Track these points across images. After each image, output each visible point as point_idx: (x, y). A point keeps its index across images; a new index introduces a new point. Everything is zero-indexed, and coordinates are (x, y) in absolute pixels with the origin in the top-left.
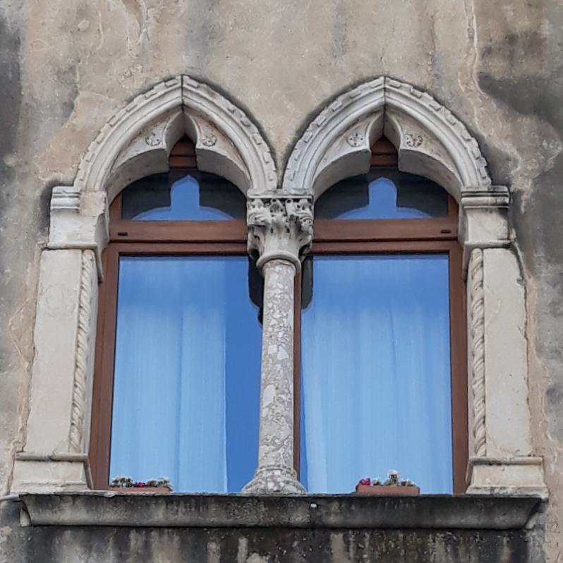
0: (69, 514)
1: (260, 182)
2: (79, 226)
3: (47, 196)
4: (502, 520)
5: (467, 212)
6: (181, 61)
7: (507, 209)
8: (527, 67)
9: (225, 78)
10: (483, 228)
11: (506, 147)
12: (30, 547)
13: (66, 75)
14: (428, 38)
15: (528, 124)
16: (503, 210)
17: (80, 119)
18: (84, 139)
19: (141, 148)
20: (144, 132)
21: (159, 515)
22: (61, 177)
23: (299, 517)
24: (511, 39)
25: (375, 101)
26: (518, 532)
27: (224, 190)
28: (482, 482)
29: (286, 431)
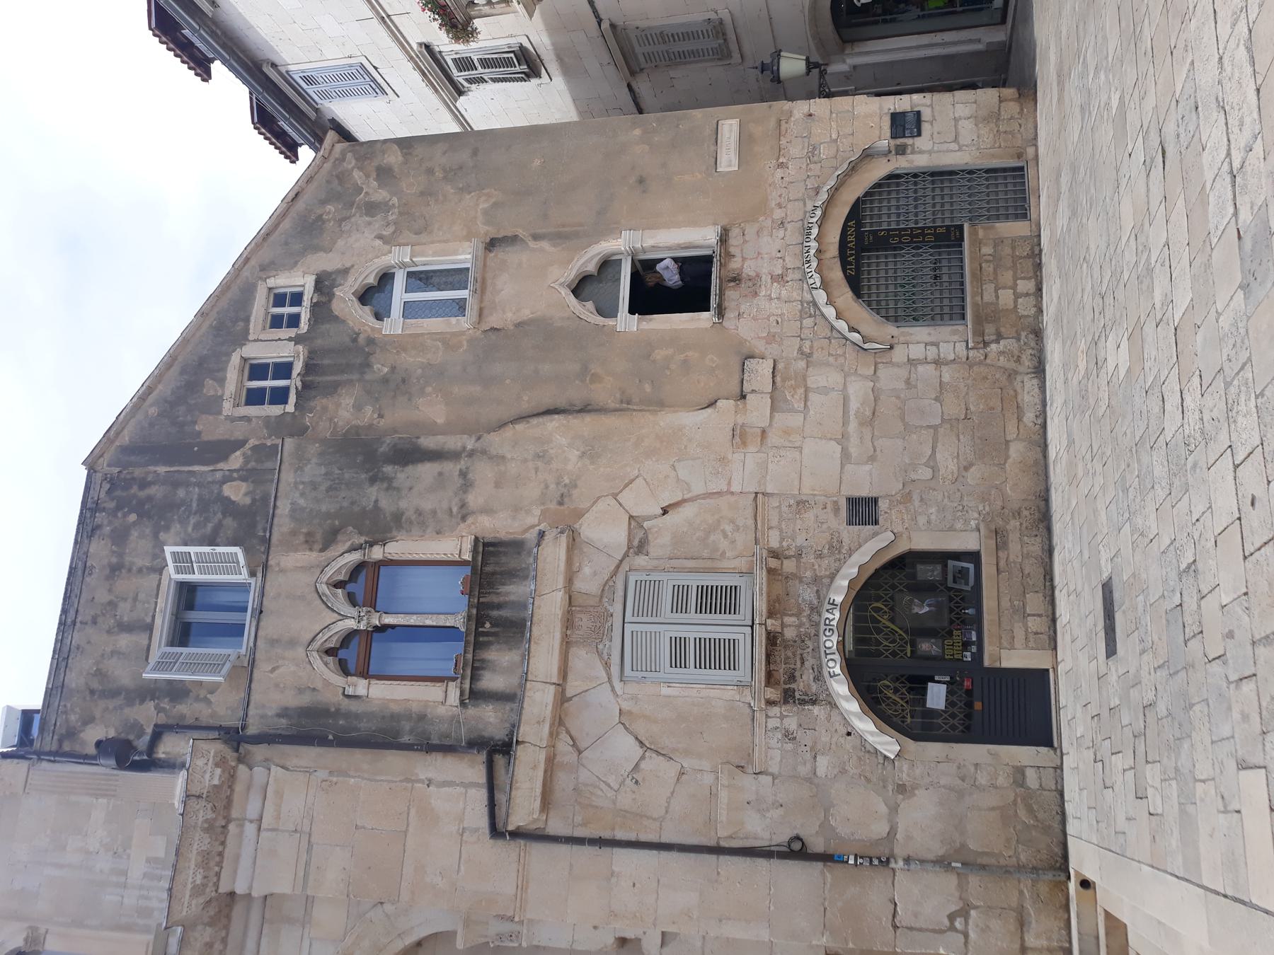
0: (467, 686)
1: (351, 624)
2: (360, 686)
3: (349, 697)
4: (481, 549)
5: (640, 751)
6: (301, 651)
7: (729, 56)
8: (319, 536)
9: (309, 636)
10: (377, 553)
11: (348, 544)
12: (477, 699)
13: (300, 691)
14: (303, 569)
15: (340, 537)
16: (371, 546)
17: (319, 685)
18: (327, 683)
19: (331, 665)
20: (326, 664)
21: (470, 656)
22: (341, 691)
23: (474, 611)
24: (307, 542)
25: (324, 587)
26: (485, 545)
27: (350, 636)
28: (467, 556)
29: (442, 617)
